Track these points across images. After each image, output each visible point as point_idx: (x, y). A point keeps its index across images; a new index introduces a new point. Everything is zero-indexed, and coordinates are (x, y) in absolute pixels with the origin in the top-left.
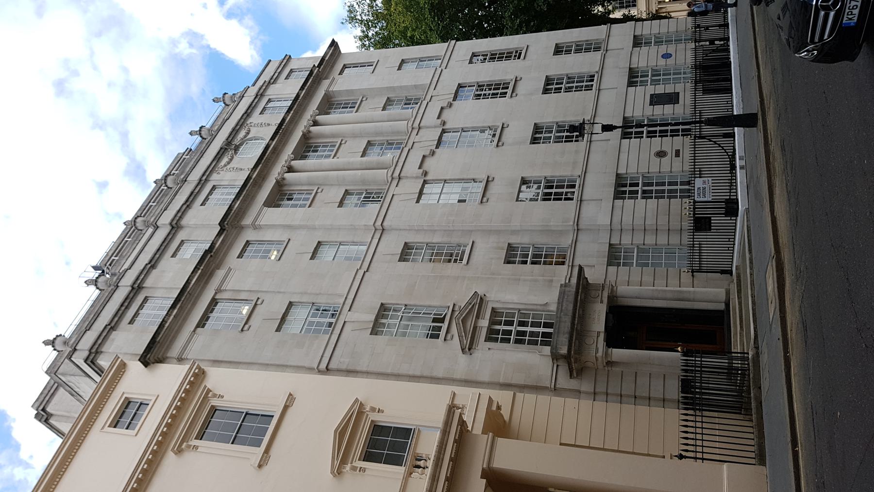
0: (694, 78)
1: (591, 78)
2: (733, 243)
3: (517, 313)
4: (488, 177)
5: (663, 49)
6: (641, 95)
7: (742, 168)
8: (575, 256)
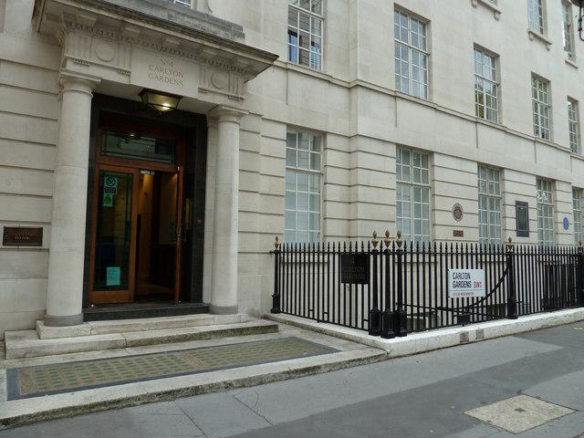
6: (531, 194)
7: (464, 335)
8: (303, 77)
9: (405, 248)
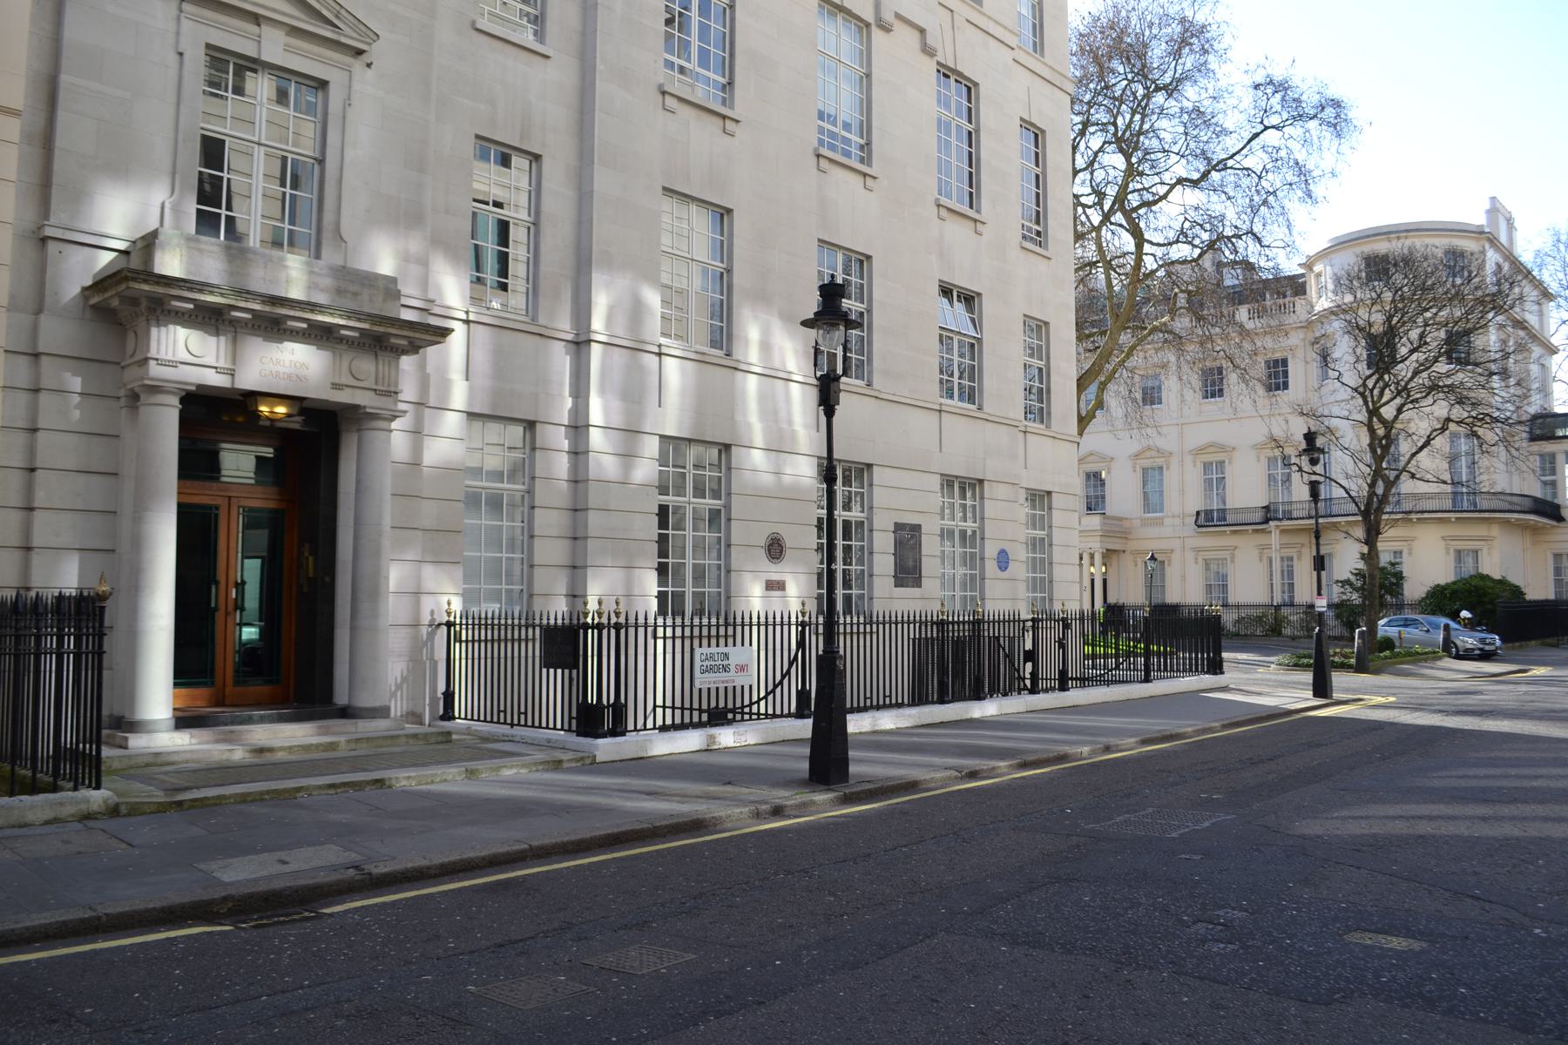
0: (950, 619)
1: (971, 396)
2: (516, 722)
3: (721, 265)
4: (875, 178)
5: (1020, 554)
9: (627, 620)
